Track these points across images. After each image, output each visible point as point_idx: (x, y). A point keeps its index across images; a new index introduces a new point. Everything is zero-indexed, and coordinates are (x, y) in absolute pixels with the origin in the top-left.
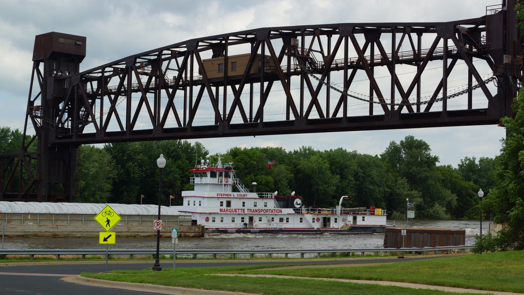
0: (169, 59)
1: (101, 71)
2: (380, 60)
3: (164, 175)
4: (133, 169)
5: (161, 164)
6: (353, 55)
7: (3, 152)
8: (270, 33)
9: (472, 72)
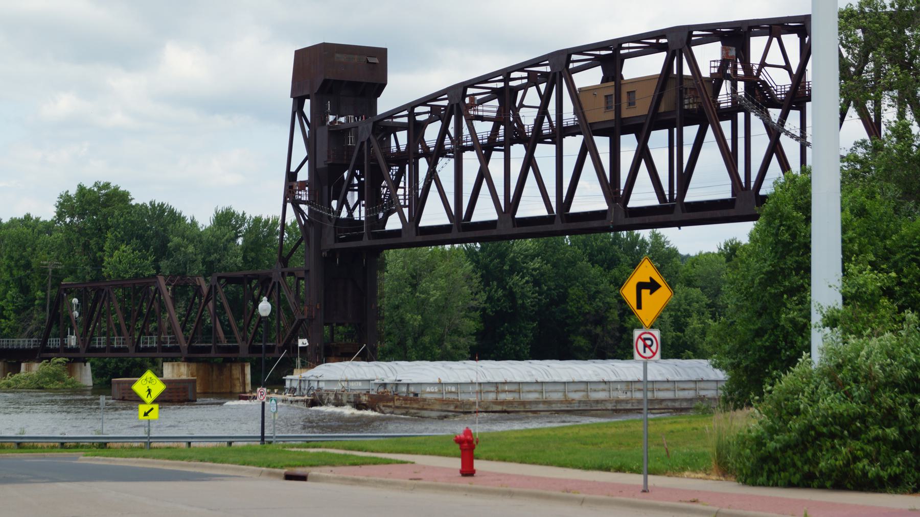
0: (525, 87)
3: (585, 299)
4: (522, 288)
5: (265, 310)
7: (268, 263)
8: (690, 35)
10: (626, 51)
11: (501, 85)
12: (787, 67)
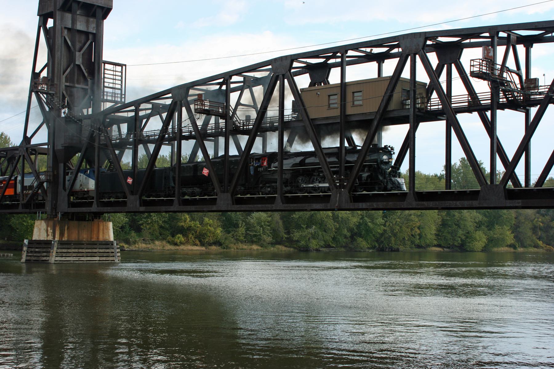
1: (135, 108)
2: (467, 104)
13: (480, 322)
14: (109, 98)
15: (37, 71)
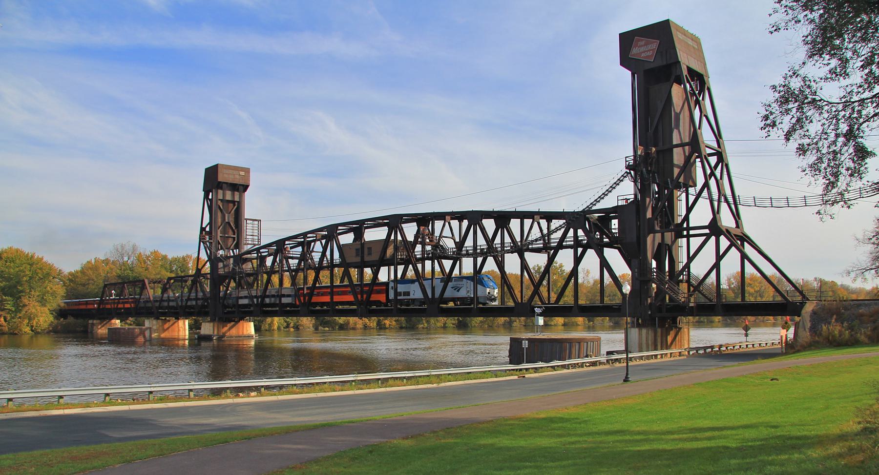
0: (314, 241)
6: (481, 242)
9: (604, 264)
10: (340, 231)
11: (302, 240)
12: (453, 238)
13: (714, 346)
14: (250, 242)
15: (204, 226)
